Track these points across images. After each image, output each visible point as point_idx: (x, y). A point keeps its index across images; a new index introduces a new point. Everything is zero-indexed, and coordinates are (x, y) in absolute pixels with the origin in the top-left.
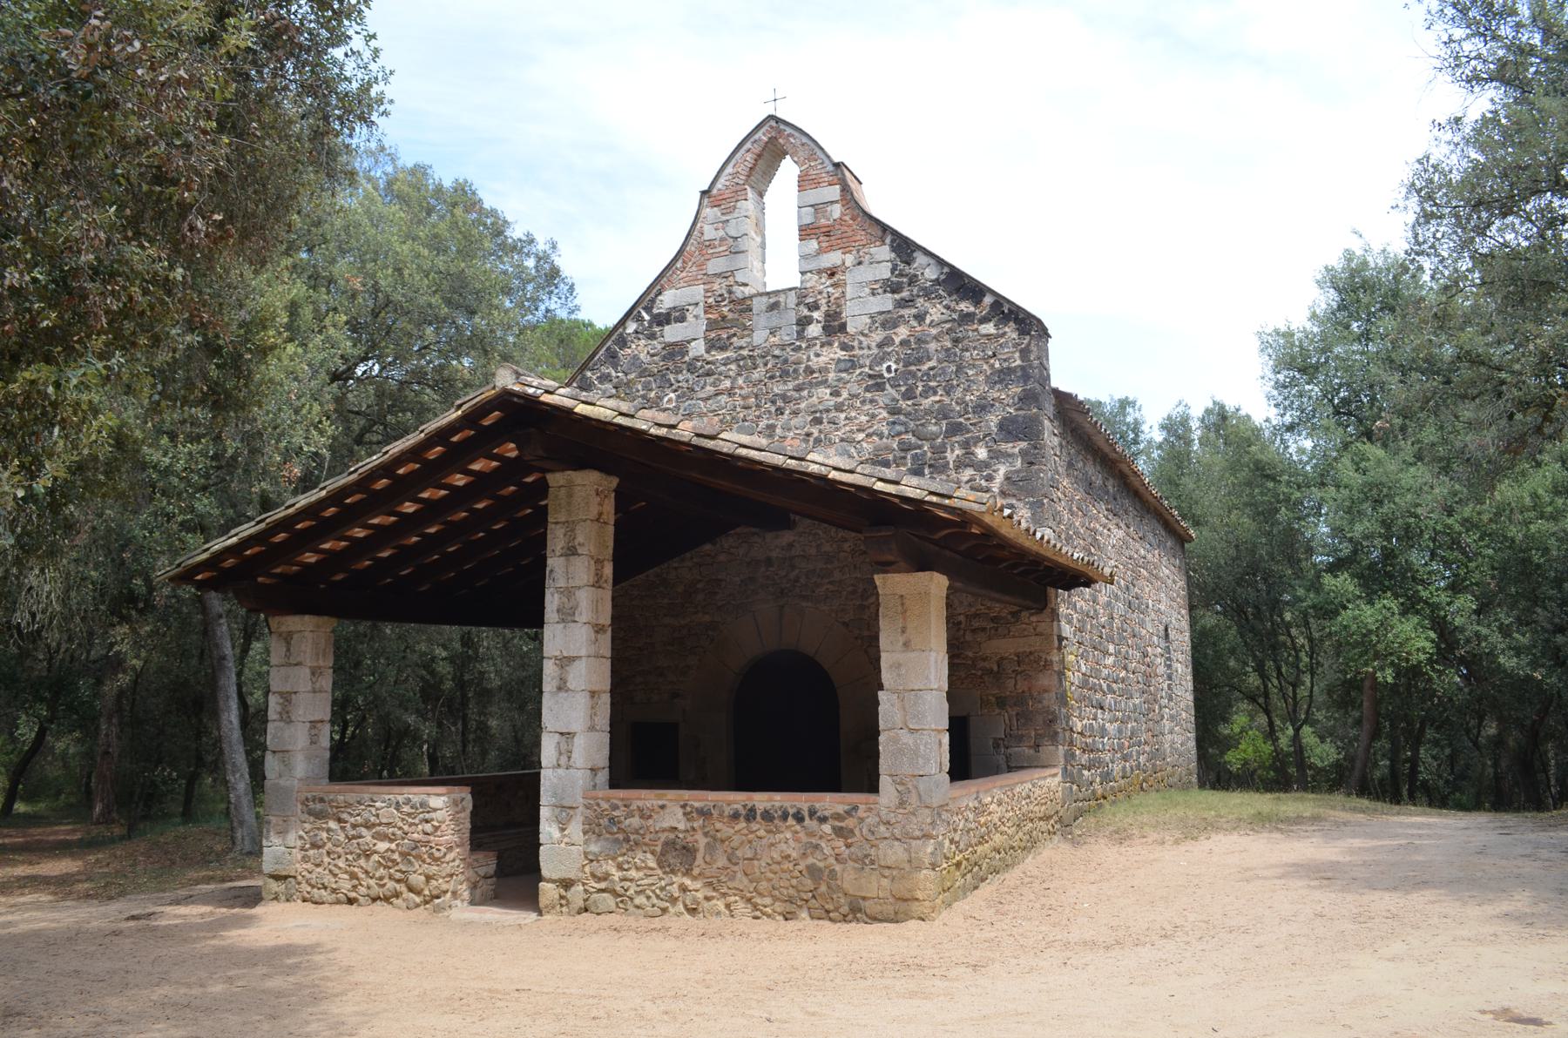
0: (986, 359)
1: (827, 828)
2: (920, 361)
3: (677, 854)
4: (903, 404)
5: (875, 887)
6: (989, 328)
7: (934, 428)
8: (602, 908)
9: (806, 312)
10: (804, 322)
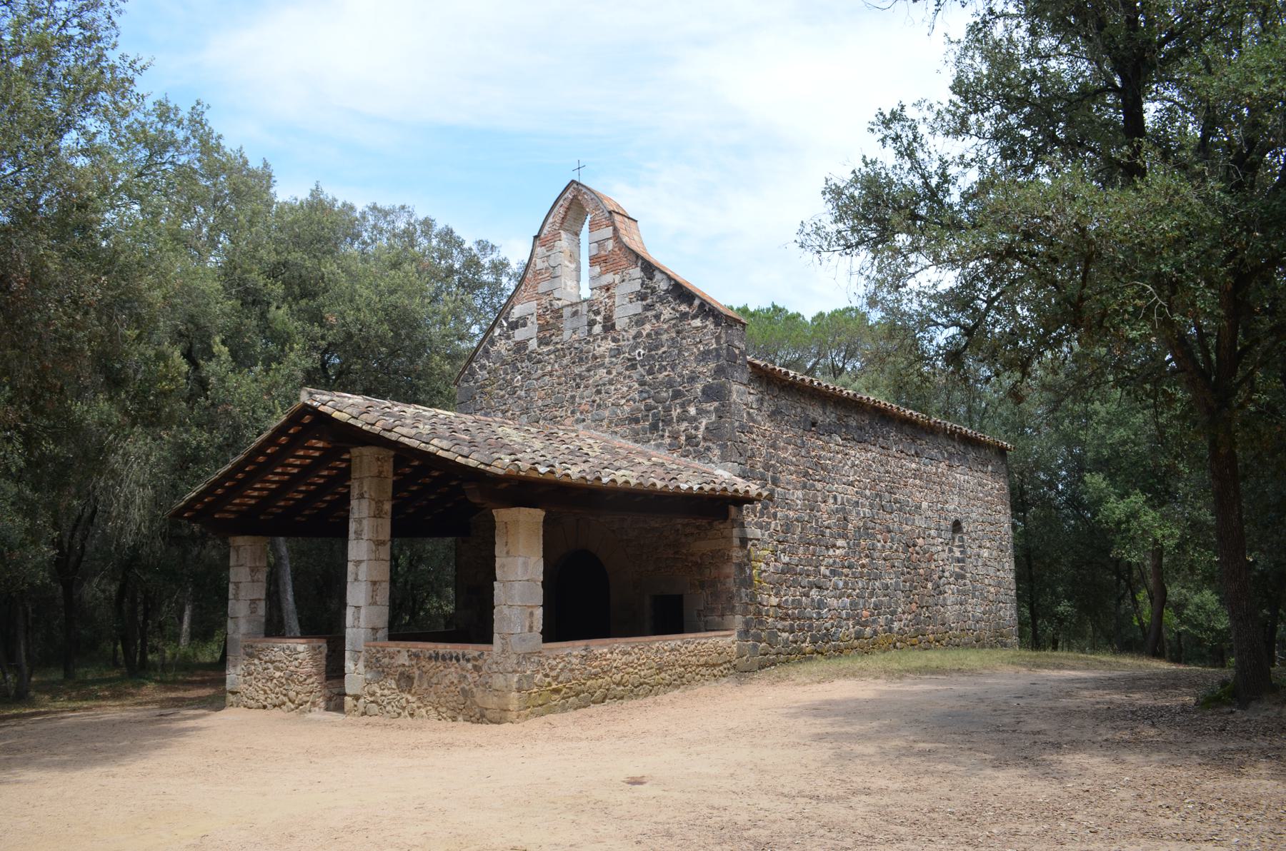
0: (696, 344)
1: (470, 666)
2: (657, 348)
3: (406, 681)
4: (648, 378)
5: (491, 702)
6: (697, 322)
7: (665, 395)
8: (372, 712)
9: (593, 317)
10: (591, 323)
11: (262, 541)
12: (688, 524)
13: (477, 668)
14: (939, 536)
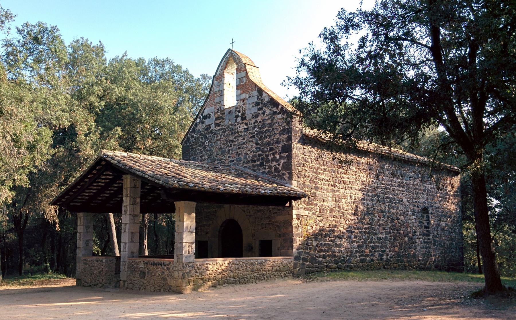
2: (263, 128)
10: (237, 116)
11: (91, 215)
12: (275, 208)
13: (168, 269)
14: (414, 215)
